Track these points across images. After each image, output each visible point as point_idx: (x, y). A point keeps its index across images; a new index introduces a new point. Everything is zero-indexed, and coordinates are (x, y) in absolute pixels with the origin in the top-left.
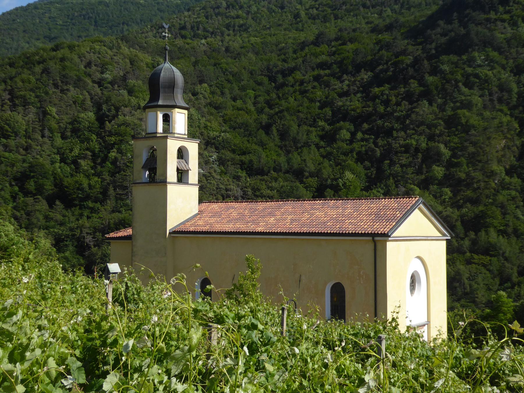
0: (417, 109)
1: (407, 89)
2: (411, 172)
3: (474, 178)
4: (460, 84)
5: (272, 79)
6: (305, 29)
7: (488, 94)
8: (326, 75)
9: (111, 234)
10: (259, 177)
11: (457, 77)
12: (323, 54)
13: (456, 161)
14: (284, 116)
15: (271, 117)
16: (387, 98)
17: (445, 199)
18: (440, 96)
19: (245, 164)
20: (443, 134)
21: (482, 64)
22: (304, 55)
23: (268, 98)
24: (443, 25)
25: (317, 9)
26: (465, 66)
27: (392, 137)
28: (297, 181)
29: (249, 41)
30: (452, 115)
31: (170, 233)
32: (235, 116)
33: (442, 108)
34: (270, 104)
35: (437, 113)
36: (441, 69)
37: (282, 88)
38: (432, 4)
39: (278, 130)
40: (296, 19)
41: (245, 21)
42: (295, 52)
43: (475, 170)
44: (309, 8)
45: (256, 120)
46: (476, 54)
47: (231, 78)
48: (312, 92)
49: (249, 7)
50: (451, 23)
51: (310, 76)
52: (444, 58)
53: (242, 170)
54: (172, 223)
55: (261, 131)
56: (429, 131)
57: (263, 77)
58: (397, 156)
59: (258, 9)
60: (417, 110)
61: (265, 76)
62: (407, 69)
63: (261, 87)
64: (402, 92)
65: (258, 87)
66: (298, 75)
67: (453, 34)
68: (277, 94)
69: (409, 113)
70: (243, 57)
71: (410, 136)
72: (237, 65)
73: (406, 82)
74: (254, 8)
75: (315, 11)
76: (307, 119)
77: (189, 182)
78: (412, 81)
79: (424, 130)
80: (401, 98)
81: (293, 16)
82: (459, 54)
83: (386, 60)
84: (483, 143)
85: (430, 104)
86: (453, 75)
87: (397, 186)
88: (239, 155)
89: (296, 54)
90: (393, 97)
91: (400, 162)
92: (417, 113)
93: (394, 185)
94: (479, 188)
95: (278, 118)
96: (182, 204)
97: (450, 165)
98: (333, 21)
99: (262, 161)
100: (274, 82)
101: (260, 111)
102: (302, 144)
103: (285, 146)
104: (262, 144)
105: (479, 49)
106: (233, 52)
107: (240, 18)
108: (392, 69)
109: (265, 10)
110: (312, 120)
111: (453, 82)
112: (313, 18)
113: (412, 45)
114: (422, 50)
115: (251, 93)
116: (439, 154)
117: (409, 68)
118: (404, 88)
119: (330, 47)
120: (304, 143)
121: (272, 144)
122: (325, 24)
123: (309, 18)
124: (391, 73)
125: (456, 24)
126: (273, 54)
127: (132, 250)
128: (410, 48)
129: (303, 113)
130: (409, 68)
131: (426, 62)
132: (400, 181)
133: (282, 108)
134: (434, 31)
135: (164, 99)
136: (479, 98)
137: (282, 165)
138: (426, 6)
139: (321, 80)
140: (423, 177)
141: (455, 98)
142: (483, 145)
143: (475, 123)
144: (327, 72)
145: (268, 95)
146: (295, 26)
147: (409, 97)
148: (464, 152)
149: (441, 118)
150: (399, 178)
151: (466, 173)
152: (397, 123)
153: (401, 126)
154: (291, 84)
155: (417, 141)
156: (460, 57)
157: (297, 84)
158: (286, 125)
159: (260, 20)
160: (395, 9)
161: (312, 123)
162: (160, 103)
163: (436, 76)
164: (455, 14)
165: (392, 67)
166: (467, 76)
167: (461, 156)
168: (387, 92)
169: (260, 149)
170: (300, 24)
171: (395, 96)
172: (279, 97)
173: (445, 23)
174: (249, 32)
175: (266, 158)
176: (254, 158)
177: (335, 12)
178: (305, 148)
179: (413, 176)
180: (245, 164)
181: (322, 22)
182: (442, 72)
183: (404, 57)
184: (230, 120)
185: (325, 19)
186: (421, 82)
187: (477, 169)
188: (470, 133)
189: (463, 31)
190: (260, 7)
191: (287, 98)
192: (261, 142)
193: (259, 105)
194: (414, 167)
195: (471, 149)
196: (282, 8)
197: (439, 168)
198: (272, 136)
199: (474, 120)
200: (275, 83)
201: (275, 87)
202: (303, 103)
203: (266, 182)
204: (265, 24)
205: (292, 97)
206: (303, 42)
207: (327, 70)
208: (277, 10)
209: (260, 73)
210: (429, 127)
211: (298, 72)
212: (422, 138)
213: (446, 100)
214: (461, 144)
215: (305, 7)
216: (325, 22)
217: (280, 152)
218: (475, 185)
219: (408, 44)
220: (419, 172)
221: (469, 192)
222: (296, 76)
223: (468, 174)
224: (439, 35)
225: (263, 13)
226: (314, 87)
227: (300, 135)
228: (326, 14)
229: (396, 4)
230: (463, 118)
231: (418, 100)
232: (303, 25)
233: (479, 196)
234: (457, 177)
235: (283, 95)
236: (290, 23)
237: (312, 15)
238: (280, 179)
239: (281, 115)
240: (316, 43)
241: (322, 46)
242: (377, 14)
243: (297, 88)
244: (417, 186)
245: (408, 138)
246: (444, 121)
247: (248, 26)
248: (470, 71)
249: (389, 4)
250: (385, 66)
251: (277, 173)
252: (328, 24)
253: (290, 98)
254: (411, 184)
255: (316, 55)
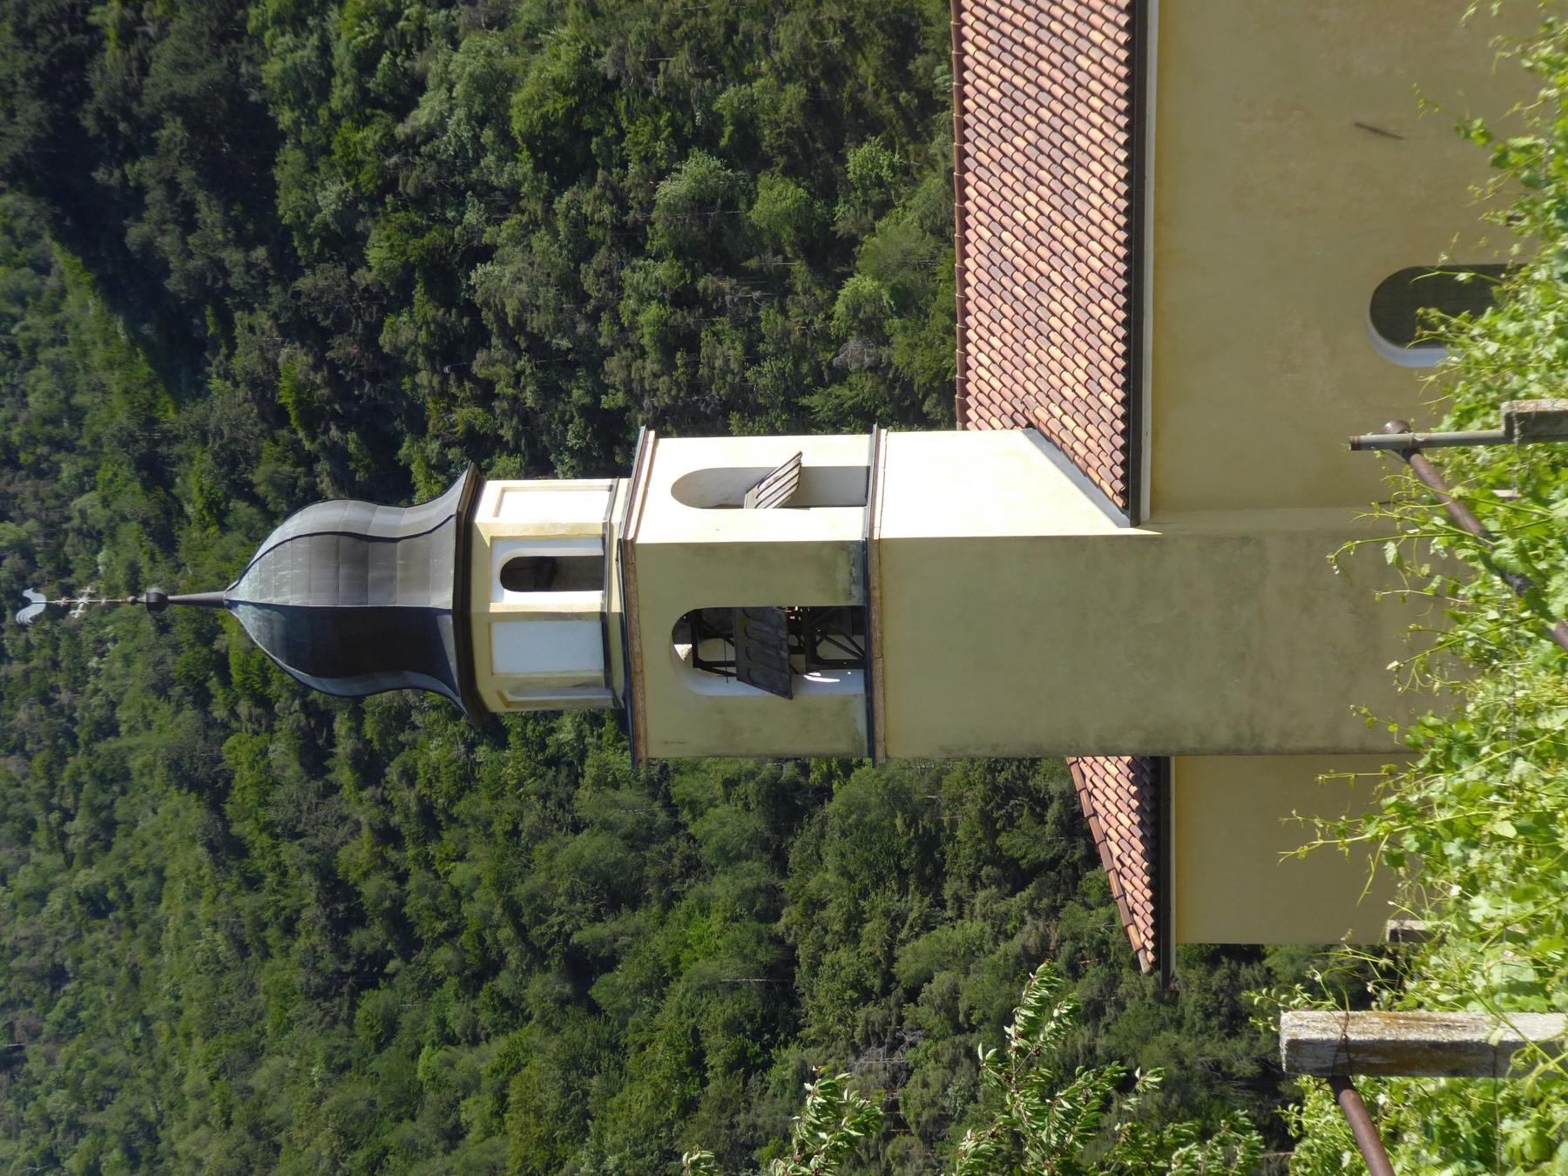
0: (508, 309)
1: (421, 360)
2: (780, 319)
3: (805, 50)
4: (401, 130)
5: (370, 973)
6: (156, 861)
7: (443, 12)
8: (357, 730)
9: (1137, 939)
10: (801, 974)
11: (370, 145)
12: (264, 753)
13: (728, 130)
14: (532, 897)
15: (537, 957)
16: (460, 443)
17: (892, 166)
18: (450, 214)
19: (744, 1050)
20: (614, 189)
21: (314, 40)
22: (265, 840)
23: (452, 982)
24: (146, 228)
25: (68, 816)
26: (323, 113)
27: (626, 409)
28: (819, 814)
29: (199, 1096)
30: (533, 155)
31: (1136, 522)
32: (531, 1118)
33: (503, 202)
34: (481, 971)
35: (525, 219)
36: (335, 214)
37: (413, 926)
38: (58, 317)
39: (597, 918)
40: (111, 907)
41: (112, 1139)
42: (252, 882)
43: (768, 46)
44: (63, 850)
45: (548, 1024)
46: (272, 70)
47: (360, 1156)
48: (430, 783)
49: (50, 1123)
50: (141, 190)
51: (360, 801)
52: (287, 204)
53: (769, 1063)
54: (1086, 516)
55: (600, 991)
56: (603, 251)
57: (360, 1014)
58: (712, 381)
59: (61, 1083)
60: (511, 307)
61: (353, 1006)
62: (333, 366)
63: (405, 1021)
64: (436, 381)
65: (404, 1036)
66: (356, 854)
67: (186, 175)
68: (437, 943)
69: (523, 345)
70: (269, 1113)
71: (624, 332)
72: (305, 1134)
73: (393, 367)
74: (58, 1101)
75: (77, 825)
76: (545, 797)
77: (865, 464)
78: (385, 340)
79: (599, 274)
80: (460, 384)
81: (97, 922)
82: (267, 140)
83: (296, 465)
84: (655, 18)
85: (486, 254)
86: (360, 164)
87: (840, 375)
88: (705, 1082)
89: (262, 878)
90: (454, 417)
91: (734, 366)
92: (524, 307)
93: (835, 389)
94: (846, 26)
95: (541, 922)
96: (971, 486)
97: (746, 152)
98: (126, 741)
99: (728, 975)
100: (384, 965)
101: (512, 1011)
102: (657, 804)
103: (664, 881)
104: (658, 983)
105: (250, 59)
106: (246, 1159)
107: (97, 1164)
108: (334, 433)
109: (63, 1053)
110: (551, 773)
111: (394, 159)
112: (107, 830)
113: (229, 357)
114: (252, 311)
115: (429, 1059)
116: (700, 203)
117: (330, 354)
118: (414, 370)
119: (234, 724)
120: (654, 796)
121: (658, 941)
122: (135, 775)
123: (108, 847)
124: (352, 435)
125: (144, 168)
126: (263, 981)
127: (1220, 753)
128: (245, 360)
129: (520, 813)
130: (330, 354)
131: (304, 283)
132: (818, 363)
133: (498, 911)
134: (174, 262)
135: (425, 583)
136: (463, 45)
137: (749, 883)
138: (64, 342)
139: (376, 745)
140: (799, 267)
141: (463, 146)
142: (664, 19)
143: (568, 54)
144: (341, 726)
145: (439, 983)
146: (139, 907)
147: (452, 351)
148: (693, 93)
149: (548, 200)
150: (805, 368)
151: (784, 81)
152: (569, 395)
153: (581, 372)
154: (392, 884)
155: (644, 299)
156: (282, 136)
157: (393, 855)
158: (573, 884)
159: (109, 1072)
160: (78, 476)
161: (564, 771)
162: (443, 599)
163: (364, 237)
164: (100, 175)
165: (327, 431)
166: (365, 106)
167: (708, 112)
168: (434, 446)
169: (679, 987)
170: (131, 885)
171: (449, 410)
172: (451, 934)
173: (140, 219)
174: (160, 1114)
175: (721, 955)
176: (720, 1011)
177: (82, 737)
178: (673, 790)
179: (793, 311)
180: (744, 1050)
181: (124, 792)
182: (348, 211)
183: (285, 383)
184: (547, 1141)
185: (116, 777)
186: (395, 296)
187: (765, 37)
188: (610, 75)
189: (172, 130)
190: (52, 1076)
191: (455, 893)
192: (647, 988)
193: (485, 1018)
194: (756, 308)
195: (680, 64)
196: (57, 976)
197: (763, 193)
198: (623, 940)
199: (554, 62)
200: (390, 956)
201: (407, 959)
202: (475, 819)
203: (823, 947)
204: (129, 1043)
205: (448, 873)
206: (212, 847)
207: (336, 726)
208: (68, 1001)
209: (341, 1027)
210: (584, 251)
211: (343, 854)
212: (630, 277)
213: (470, 186)
214: (657, 112)
215: (55, 872)
216: (126, 775)
217: (690, 900)
218: (835, 42)
219: (227, 375)
220: (777, 286)
221: (863, 69)
222: (357, 866)
223: (785, 75)
224: (190, 239)
225: (80, 1062)
226: (410, 776)
227: (614, 815)
228: (93, 774)
229: (55, 470)
230: (549, 107)
231: (472, 310)
232: (137, 872)
233: (880, 26)
234: (799, 120)
235: (443, 916)
236: (127, 932)
237: (95, 838)
238: (813, 884)
239: (526, 911)
240: (212, 788)
241: (229, 760)
242: (96, 552)
243: (411, 852)
244: (840, 286)
245: (633, 338)
246: (559, 188)
247: (133, 1127)
248: (349, 90)
249: (52, 502)
250: (323, 466)
251: (784, 903)
252: (135, 763)
253: (455, 880)
254: (829, 317)
255: (269, 782)
